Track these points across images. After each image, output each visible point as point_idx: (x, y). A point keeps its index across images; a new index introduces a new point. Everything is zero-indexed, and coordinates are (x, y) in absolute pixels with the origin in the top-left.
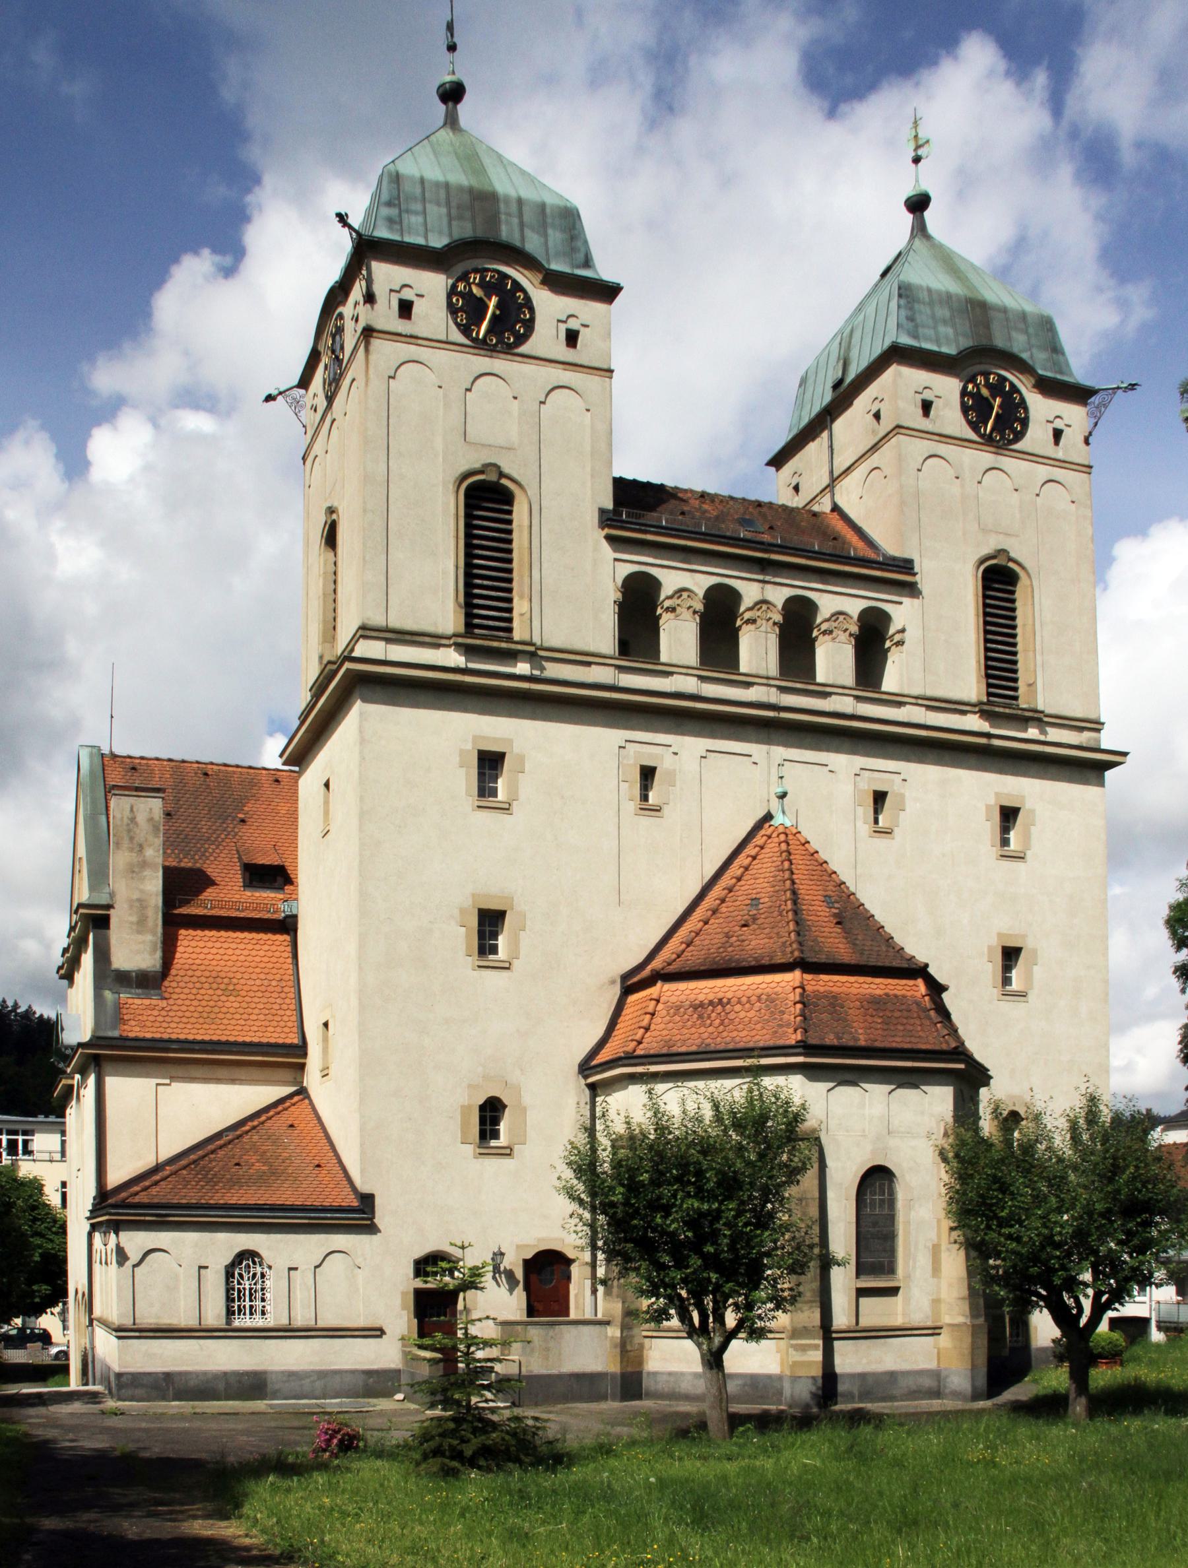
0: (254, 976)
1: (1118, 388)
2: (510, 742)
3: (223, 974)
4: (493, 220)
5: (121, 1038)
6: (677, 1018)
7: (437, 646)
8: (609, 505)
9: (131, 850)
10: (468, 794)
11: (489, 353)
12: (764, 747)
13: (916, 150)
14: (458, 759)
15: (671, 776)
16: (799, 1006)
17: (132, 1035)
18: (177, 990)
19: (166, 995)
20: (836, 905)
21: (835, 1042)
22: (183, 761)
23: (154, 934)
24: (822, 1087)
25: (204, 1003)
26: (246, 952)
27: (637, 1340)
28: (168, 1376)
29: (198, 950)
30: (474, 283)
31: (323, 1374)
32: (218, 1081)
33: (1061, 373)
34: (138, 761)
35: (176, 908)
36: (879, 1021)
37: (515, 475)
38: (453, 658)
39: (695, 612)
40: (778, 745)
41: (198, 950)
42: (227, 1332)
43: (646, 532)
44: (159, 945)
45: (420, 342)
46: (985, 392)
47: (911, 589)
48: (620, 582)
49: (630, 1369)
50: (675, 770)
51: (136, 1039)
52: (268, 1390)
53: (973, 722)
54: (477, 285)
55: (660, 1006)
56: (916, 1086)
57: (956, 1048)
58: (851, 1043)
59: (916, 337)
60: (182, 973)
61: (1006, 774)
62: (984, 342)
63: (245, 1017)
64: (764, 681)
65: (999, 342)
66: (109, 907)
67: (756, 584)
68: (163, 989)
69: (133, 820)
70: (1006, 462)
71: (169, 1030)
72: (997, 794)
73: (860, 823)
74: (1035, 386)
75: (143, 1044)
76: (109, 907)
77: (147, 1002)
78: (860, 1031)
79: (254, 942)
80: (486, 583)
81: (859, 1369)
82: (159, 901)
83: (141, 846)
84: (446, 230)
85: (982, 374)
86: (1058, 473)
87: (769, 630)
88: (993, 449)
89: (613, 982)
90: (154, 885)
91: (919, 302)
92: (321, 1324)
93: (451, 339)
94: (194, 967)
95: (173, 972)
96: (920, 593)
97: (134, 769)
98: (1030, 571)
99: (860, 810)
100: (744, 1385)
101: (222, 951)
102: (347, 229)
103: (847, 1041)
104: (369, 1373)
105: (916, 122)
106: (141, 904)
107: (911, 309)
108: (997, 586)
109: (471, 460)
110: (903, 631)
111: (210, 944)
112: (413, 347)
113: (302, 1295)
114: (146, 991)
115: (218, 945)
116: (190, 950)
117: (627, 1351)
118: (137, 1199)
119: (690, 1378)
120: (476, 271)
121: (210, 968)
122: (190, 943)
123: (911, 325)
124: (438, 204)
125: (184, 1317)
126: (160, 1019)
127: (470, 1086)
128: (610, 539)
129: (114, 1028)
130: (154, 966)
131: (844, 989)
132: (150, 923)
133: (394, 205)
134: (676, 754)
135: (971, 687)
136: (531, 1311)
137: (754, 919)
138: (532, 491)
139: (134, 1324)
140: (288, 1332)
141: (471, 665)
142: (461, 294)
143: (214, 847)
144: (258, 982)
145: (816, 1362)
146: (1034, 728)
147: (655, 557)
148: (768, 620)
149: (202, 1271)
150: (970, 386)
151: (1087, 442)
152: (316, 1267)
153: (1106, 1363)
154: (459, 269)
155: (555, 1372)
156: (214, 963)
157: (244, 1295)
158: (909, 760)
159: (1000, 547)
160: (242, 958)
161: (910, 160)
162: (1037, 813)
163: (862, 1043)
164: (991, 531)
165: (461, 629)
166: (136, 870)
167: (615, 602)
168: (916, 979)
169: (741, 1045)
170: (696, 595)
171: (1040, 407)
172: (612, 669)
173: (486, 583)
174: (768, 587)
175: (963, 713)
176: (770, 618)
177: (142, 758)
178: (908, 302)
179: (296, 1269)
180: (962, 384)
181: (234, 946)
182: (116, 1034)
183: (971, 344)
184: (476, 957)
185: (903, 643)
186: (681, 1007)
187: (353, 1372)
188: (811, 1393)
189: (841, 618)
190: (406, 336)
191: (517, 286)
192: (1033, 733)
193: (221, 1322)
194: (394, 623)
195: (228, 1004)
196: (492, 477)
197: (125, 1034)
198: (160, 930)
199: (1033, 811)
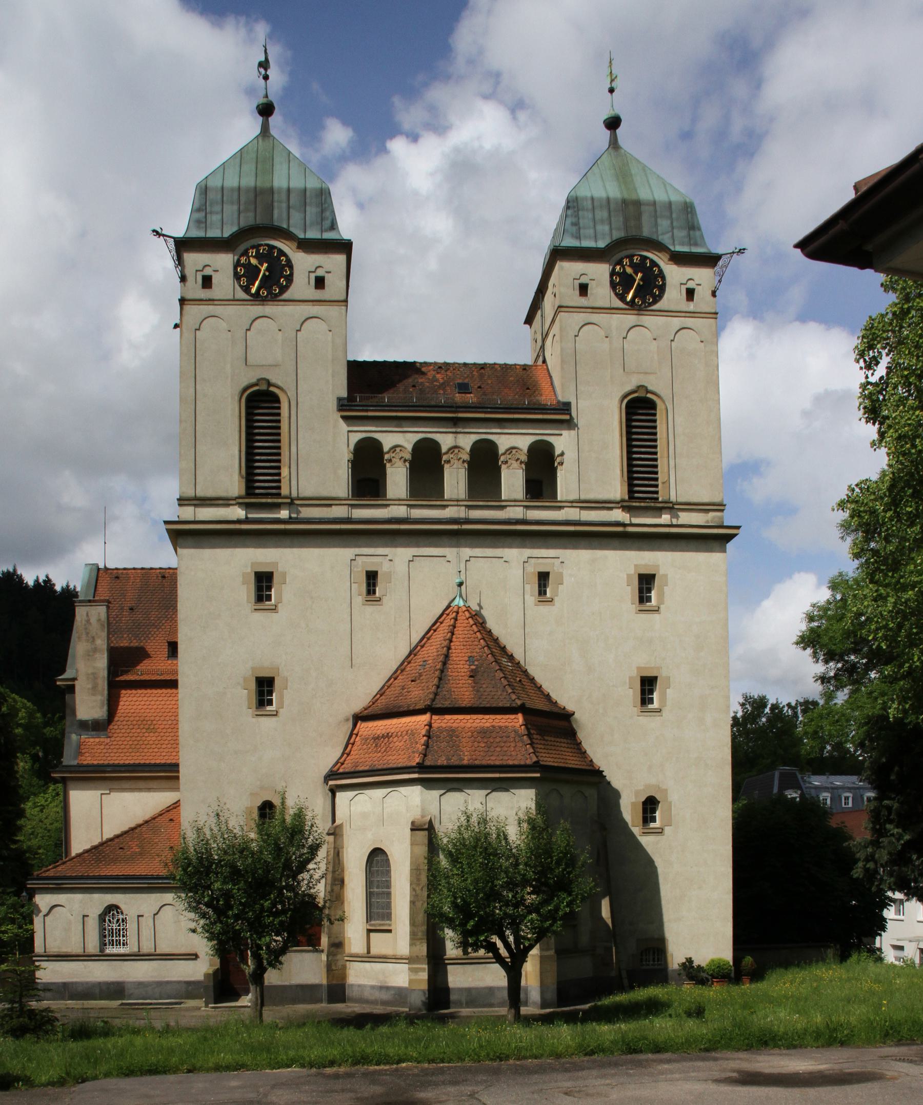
0: (167, 718)
1: (733, 253)
2: (276, 564)
3: (147, 718)
4: (270, 208)
5: (79, 766)
6: (365, 747)
7: (228, 505)
8: (344, 394)
9: (88, 641)
10: (248, 602)
11: (262, 303)
12: (455, 550)
13: (611, 83)
14: (241, 579)
15: (389, 575)
16: (425, 738)
17: (85, 763)
18: (118, 731)
19: (110, 735)
20: (476, 663)
21: (445, 763)
22: (151, 569)
23: (103, 695)
24: (436, 793)
25: (134, 739)
26: (163, 703)
27: (340, 963)
28: (65, 985)
29: (133, 703)
30: (252, 256)
31: (160, 984)
32: (140, 790)
33: (696, 244)
34: (121, 571)
35: (118, 676)
36: (483, 745)
37: (280, 383)
38: (239, 513)
39: (405, 461)
40: (465, 547)
41: (133, 703)
42: (101, 956)
43: (367, 411)
44: (106, 702)
45: (216, 303)
46: (629, 270)
47: (569, 424)
48: (352, 447)
49: (334, 982)
50: (391, 572)
51: (88, 766)
52: (126, 994)
53: (618, 515)
54: (254, 257)
55: (358, 738)
56: (507, 790)
57: (535, 762)
58: (457, 763)
59: (578, 237)
60: (122, 719)
61: (644, 550)
62: (633, 232)
63: (159, 746)
64: (455, 503)
65: (646, 232)
66: (74, 679)
67: (451, 435)
68: (109, 730)
69: (88, 621)
70: (647, 320)
71: (109, 758)
72: (636, 566)
73: (527, 597)
74: (671, 259)
75: (90, 769)
76: (74, 679)
77: (97, 740)
78: (466, 753)
79: (168, 695)
80: (263, 458)
81: (466, 985)
82: (105, 673)
83: (93, 638)
84: (236, 221)
85: (627, 257)
86: (689, 322)
87: (460, 466)
88: (636, 312)
89: (347, 720)
90: (102, 663)
91: (583, 209)
92: (158, 952)
93: (237, 297)
94: (130, 715)
95: (116, 719)
96: (577, 425)
97: (117, 577)
98: (664, 398)
99: (528, 587)
100: (395, 994)
101: (148, 703)
102: (161, 237)
103: (454, 761)
104: (188, 983)
105: (611, 62)
106: (94, 676)
107: (577, 216)
108: (641, 412)
109: (248, 377)
110: (562, 454)
111: (140, 699)
112: (211, 307)
113: (147, 933)
114: (97, 733)
115: (145, 699)
116: (127, 703)
117: (333, 970)
118: (47, 874)
119: (369, 988)
120: (252, 247)
121: (140, 715)
122: (130, 701)
123: (574, 229)
124: (232, 203)
125: (74, 947)
126: (105, 751)
127: (251, 794)
128: (343, 417)
129: (76, 758)
130: (103, 716)
131: (462, 724)
132: (100, 688)
133: (203, 210)
134: (391, 560)
135: (616, 489)
136: (313, 942)
137: (420, 675)
138: (291, 394)
139: (45, 952)
140: (138, 956)
141: (253, 516)
142: (243, 265)
143: (155, 630)
144: (170, 722)
145: (422, 980)
146: (665, 514)
147: (377, 426)
148: (459, 460)
149: (86, 918)
150: (618, 268)
151: (714, 294)
152: (155, 915)
153: (717, 982)
154: (242, 248)
155: (287, 983)
156: (143, 711)
157: (116, 933)
158: (566, 548)
159: (639, 384)
160: (160, 707)
161: (607, 90)
162: (669, 576)
163: (465, 762)
164: (634, 372)
165: (243, 492)
166: (91, 654)
167: (348, 461)
168: (517, 714)
169: (391, 766)
170: (406, 448)
171: (675, 275)
172: (346, 507)
173: (263, 458)
174: (460, 436)
175: (611, 509)
176: (460, 458)
177: (125, 569)
178: (575, 212)
179: (142, 916)
180: (611, 267)
181: (155, 699)
182: (75, 763)
183: (623, 235)
184: (255, 709)
185: (562, 463)
186: (368, 739)
187: (179, 982)
188: (422, 1001)
189: (514, 451)
190: (206, 300)
191: (282, 253)
192: (665, 518)
193: (96, 951)
194: (200, 493)
195: (149, 739)
196: (264, 387)
197: (80, 762)
198: (106, 692)
199: (666, 576)
